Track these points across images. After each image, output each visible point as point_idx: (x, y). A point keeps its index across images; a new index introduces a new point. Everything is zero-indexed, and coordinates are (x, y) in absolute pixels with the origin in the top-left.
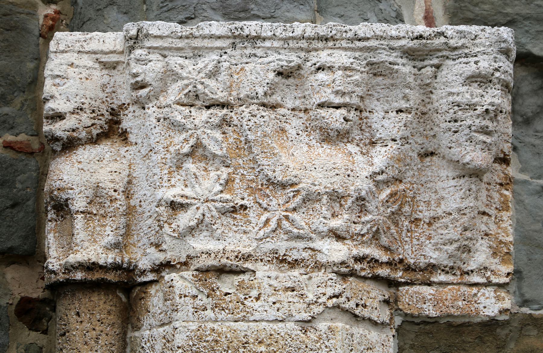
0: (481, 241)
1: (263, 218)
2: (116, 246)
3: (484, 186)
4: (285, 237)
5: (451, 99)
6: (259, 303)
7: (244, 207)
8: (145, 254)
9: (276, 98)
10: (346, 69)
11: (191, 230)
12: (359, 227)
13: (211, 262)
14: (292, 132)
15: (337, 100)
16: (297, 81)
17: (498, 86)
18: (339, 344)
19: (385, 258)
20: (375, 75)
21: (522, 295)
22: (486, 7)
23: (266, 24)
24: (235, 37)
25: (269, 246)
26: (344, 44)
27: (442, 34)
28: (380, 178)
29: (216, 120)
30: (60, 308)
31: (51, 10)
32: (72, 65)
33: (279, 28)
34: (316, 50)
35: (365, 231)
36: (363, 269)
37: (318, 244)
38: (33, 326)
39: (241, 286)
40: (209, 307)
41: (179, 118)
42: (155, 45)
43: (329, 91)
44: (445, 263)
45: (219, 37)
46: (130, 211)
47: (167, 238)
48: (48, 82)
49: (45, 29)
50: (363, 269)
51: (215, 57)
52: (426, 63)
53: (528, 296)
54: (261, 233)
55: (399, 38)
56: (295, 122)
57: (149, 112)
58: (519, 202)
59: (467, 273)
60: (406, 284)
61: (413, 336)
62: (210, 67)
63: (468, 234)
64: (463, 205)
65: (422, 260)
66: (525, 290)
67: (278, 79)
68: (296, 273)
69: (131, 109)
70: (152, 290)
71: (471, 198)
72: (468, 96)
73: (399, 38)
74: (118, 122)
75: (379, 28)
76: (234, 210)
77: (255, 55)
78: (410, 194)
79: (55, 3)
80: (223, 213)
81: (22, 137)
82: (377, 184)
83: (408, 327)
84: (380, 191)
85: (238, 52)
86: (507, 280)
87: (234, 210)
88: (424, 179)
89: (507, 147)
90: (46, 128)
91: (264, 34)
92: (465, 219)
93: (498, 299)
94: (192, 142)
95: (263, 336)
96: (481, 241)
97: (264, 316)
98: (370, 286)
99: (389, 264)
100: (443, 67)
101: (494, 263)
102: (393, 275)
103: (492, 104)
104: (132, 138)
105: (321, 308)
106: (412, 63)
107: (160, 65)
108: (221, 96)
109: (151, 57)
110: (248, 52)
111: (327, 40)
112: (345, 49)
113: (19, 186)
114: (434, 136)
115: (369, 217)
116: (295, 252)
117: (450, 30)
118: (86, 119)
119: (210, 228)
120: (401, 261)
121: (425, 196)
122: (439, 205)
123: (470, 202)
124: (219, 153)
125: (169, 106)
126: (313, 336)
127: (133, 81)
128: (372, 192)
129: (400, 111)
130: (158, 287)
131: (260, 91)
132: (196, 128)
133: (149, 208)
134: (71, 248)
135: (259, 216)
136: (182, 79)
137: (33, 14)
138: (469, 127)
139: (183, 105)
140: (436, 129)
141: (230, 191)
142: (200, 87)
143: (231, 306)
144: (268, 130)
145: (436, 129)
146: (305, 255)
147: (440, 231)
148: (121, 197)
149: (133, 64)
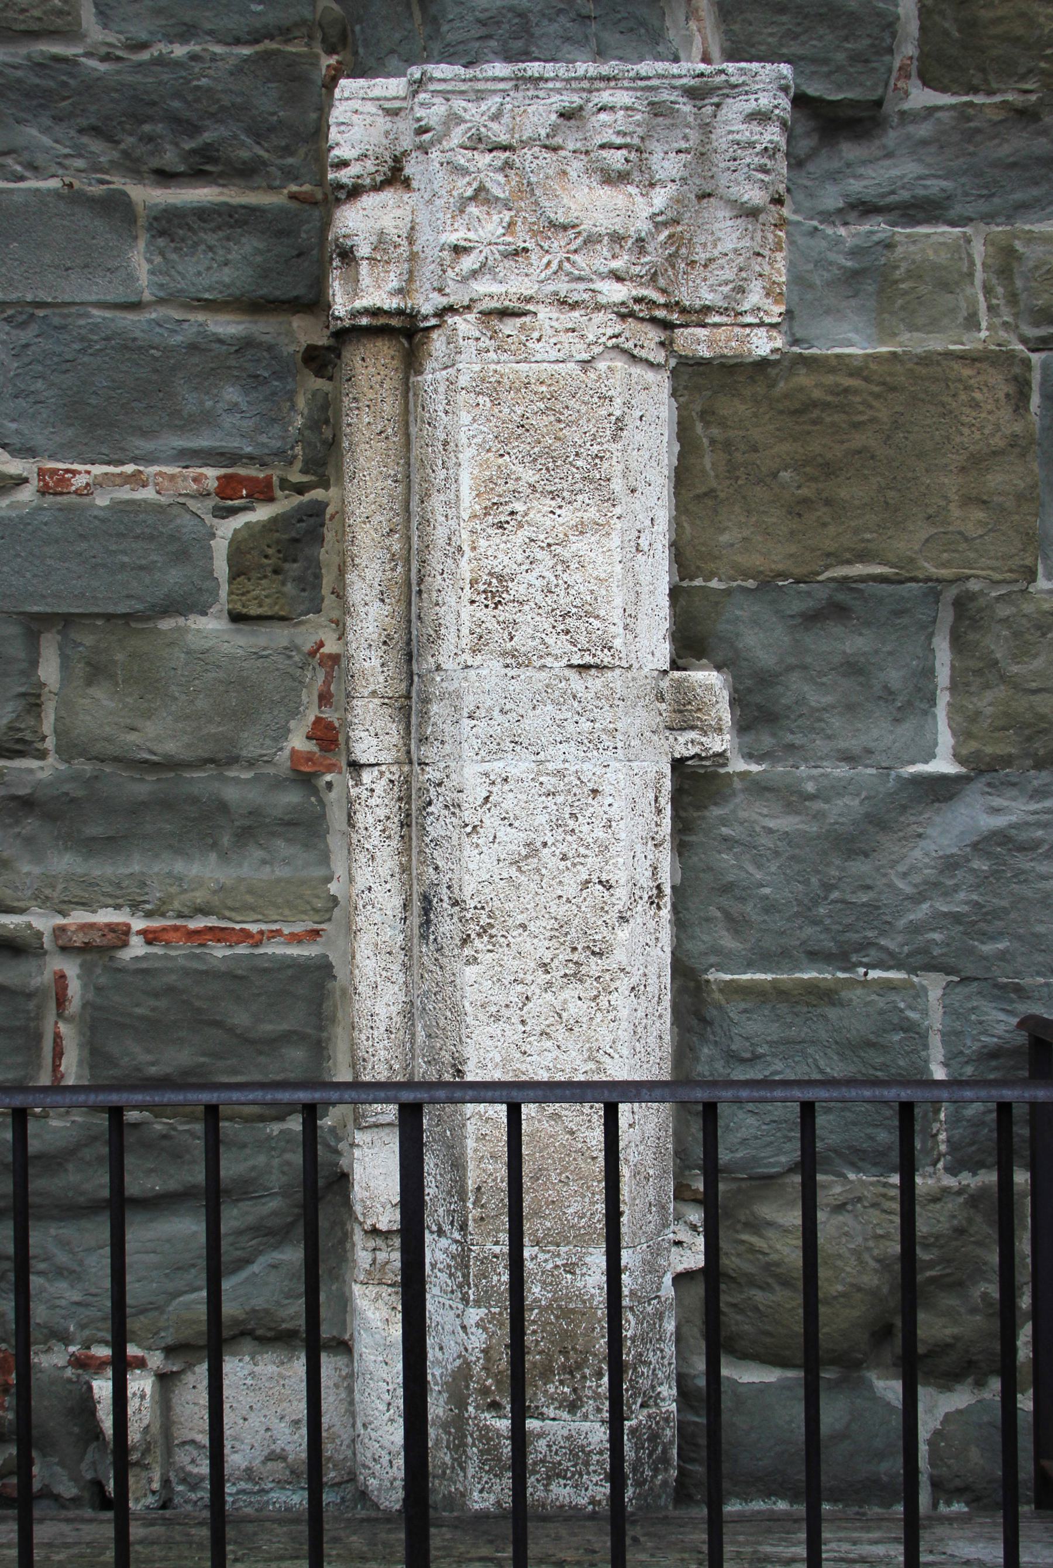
0: (754, 282)
1: (545, 260)
2: (400, 291)
3: (759, 226)
4: (566, 279)
5: (730, 137)
6: (541, 344)
7: (526, 250)
8: (427, 299)
9: (558, 140)
10: (627, 109)
11: (474, 274)
12: (638, 268)
13: (494, 304)
14: (573, 175)
15: (619, 141)
16: (578, 123)
17: (777, 124)
18: (618, 383)
19: (662, 300)
20: (656, 115)
21: (793, 335)
22: (763, 48)
23: (549, 66)
24: (518, 79)
25: (550, 288)
26: (626, 84)
27: (722, 72)
28: (659, 219)
29: (498, 163)
30: (346, 354)
31: (333, 60)
32: (356, 112)
33: (561, 69)
34: (598, 90)
35: (643, 272)
36: (641, 311)
37: (599, 285)
38: (319, 373)
39: (523, 328)
40: (492, 349)
41: (462, 161)
42: (439, 88)
43: (611, 131)
44: (720, 304)
45: (502, 79)
46: (413, 257)
47: (450, 282)
48: (333, 130)
49: (328, 79)
50: (641, 311)
51: (498, 100)
52: (707, 101)
53: (798, 336)
54: (543, 275)
55: (680, 77)
56: (576, 164)
57: (433, 156)
58: (792, 243)
59: (741, 314)
60: (681, 326)
61: (686, 377)
62: (493, 110)
63: (744, 275)
64: (739, 246)
65: (698, 302)
66: (796, 329)
67: (560, 121)
68: (576, 314)
69: (414, 154)
70: (435, 335)
71: (747, 238)
72: (748, 134)
73: (680, 77)
74: (401, 169)
75: (661, 67)
76: (516, 253)
77: (537, 97)
78: (687, 236)
79: (337, 53)
80: (506, 255)
81: (307, 188)
82: (657, 225)
83: (682, 369)
84: (659, 232)
85: (520, 95)
86: (779, 320)
87: (516, 253)
88: (700, 221)
89: (782, 188)
90: (331, 176)
91: (546, 75)
92: (741, 259)
93: (770, 338)
94: (475, 185)
95: (544, 376)
96: (754, 282)
97: (545, 357)
98: (647, 327)
99: (666, 306)
100: (724, 106)
101: (768, 304)
102: (669, 317)
103: (771, 142)
104: (415, 184)
105: (601, 348)
106: (692, 102)
107: (443, 109)
108: (504, 138)
109: (435, 100)
110: (530, 93)
111: (609, 79)
112: (627, 89)
113: (304, 235)
114: (712, 177)
115: (648, 259)
116: (575, 293)
117: (731, 67)
118: (370, 165)
119: (492, 271)
120: (677, 303)
121: (701, 238)
122: (715, 246)
123: (746, 242)
124: (502, 196)
125: (452, 150)
126: (592, 375)
127: (416, 126)
128: (651, 233)
129: (679, 151)
130: (440, 331)
131: (543, 133)
132: (479, 171)
133: (432, 253)
134: (356, 294)
135: (541, 258)
136: (466, 122)
137: (316, 65)
138: (748, 165)
139: (466, 148)
140: (714, 169)
141: (512, 234)
142: (483, 130)
143: (513, 347)
144: (551, 172)
145: (714, 169)
146: (586, 296)
147: (716, 272)
148: (405, 243)
149: (416, 108)
